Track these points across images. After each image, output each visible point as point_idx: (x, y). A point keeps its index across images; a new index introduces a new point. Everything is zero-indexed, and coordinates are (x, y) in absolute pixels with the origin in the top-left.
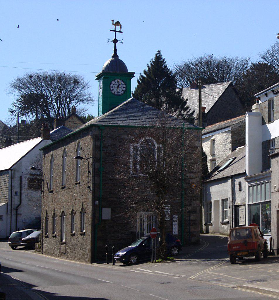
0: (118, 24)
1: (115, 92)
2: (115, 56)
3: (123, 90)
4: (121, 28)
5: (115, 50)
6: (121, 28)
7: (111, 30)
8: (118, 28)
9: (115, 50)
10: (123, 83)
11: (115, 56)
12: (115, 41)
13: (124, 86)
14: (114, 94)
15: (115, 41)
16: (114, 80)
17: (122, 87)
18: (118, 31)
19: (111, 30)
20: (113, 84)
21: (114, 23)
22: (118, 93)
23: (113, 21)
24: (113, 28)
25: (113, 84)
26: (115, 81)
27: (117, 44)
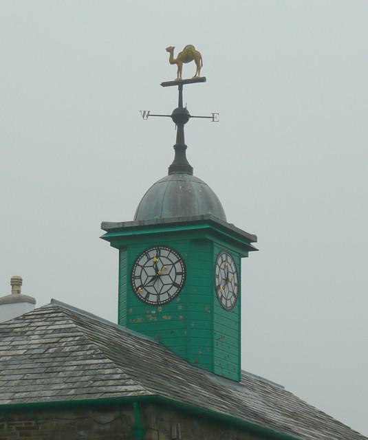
0: (190, 55)
1: (177, 274)
2: (180, 166)
3: (174, 284)
4: (199, 68)
5: (180, 148)
6: (199, 68)
7: (164, 84)
8: (189, 70)
9: (180, 148)
10: (174, 259)
11: (180, 166)
12: (181, 117)
13: (179, 267)
14: (184, 273)
15: (181, 117)
16: (145, 252)
17: (173, 274)
18: (173, 80)
19: (164, 84)
20: (143, 267)
21: (175, 57)
22: (158, 295)
23: (171, 50)
24: (171, 73)
25: (143, 267)
26: (159, 250)
27: (186, 127)
